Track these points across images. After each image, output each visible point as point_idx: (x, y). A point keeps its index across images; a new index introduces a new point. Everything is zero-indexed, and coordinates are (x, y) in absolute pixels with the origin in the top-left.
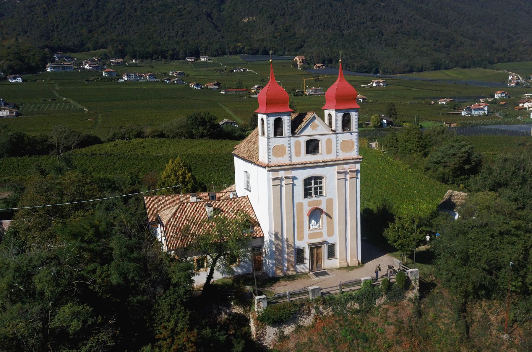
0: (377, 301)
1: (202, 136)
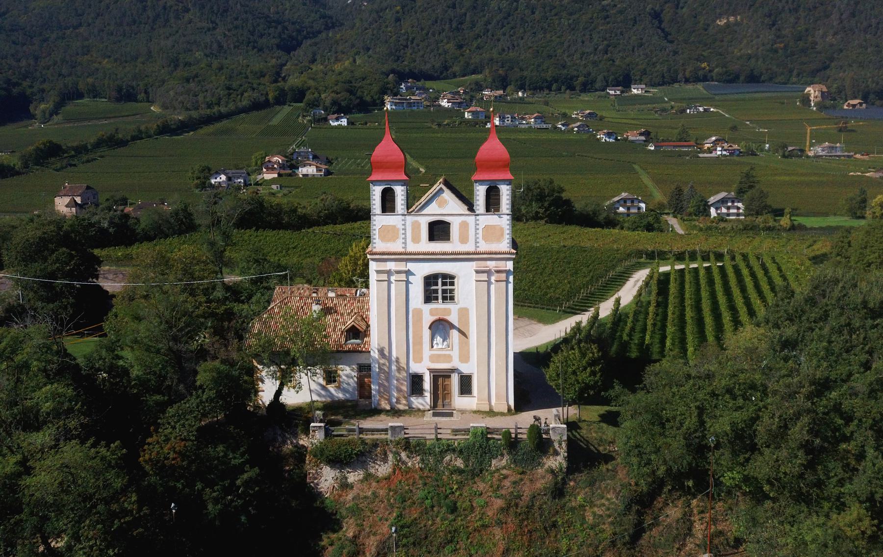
0: (494, 462)
1: (536, 217)
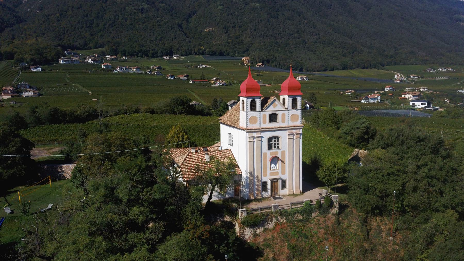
0: (313, 214)
1: (181, 113)
